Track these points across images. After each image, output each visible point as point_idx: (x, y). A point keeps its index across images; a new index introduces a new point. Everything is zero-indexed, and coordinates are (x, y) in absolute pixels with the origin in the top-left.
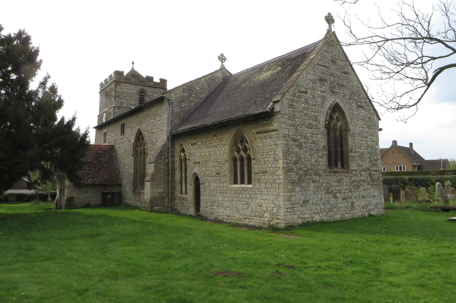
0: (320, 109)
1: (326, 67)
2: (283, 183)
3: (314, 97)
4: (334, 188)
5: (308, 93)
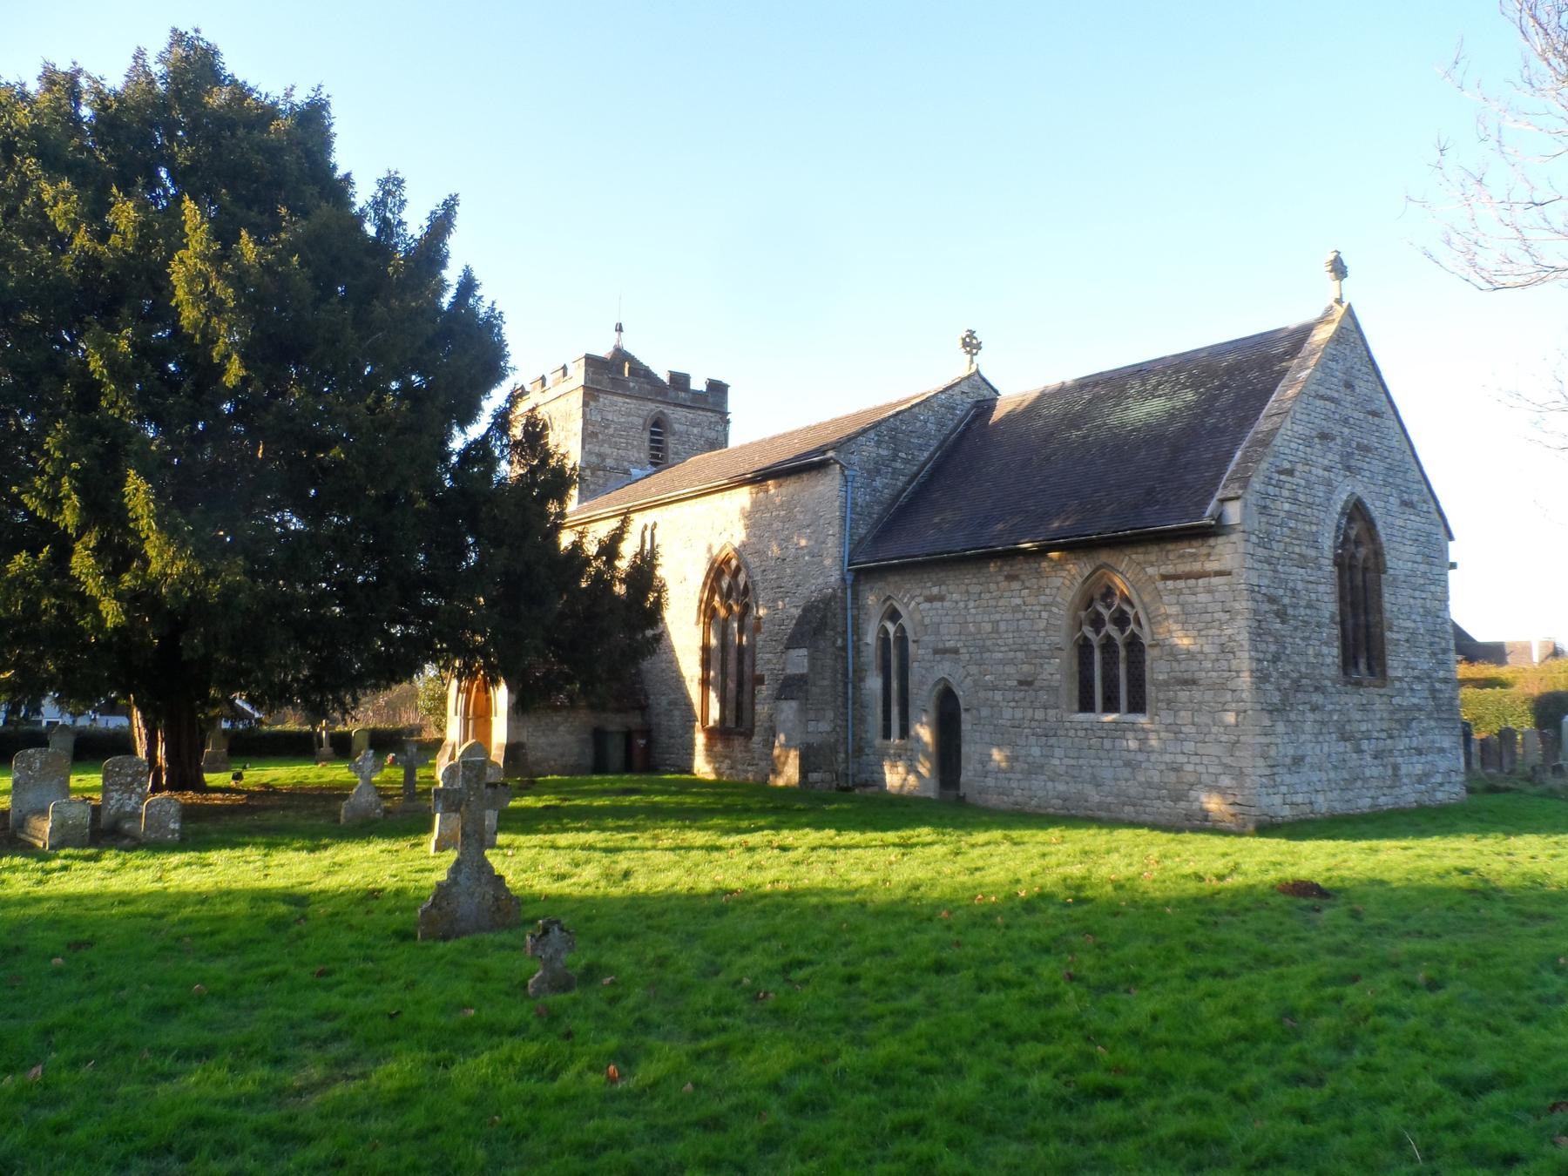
0: (1322, 515)
1: (1332, 400)
2: (1250, 712)
3: (1309, 485)
4: (1355, 726)
5: (1297, 474)
